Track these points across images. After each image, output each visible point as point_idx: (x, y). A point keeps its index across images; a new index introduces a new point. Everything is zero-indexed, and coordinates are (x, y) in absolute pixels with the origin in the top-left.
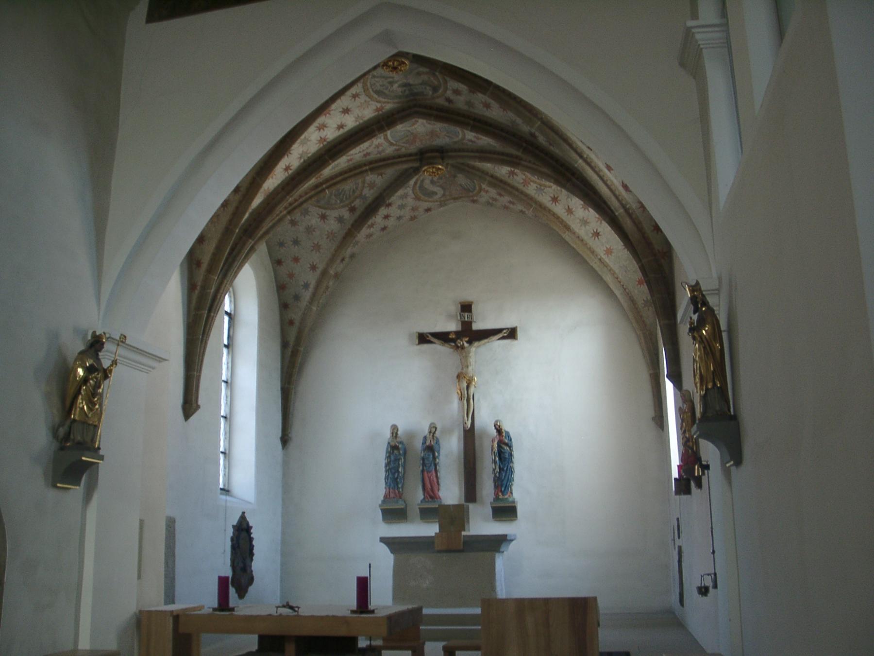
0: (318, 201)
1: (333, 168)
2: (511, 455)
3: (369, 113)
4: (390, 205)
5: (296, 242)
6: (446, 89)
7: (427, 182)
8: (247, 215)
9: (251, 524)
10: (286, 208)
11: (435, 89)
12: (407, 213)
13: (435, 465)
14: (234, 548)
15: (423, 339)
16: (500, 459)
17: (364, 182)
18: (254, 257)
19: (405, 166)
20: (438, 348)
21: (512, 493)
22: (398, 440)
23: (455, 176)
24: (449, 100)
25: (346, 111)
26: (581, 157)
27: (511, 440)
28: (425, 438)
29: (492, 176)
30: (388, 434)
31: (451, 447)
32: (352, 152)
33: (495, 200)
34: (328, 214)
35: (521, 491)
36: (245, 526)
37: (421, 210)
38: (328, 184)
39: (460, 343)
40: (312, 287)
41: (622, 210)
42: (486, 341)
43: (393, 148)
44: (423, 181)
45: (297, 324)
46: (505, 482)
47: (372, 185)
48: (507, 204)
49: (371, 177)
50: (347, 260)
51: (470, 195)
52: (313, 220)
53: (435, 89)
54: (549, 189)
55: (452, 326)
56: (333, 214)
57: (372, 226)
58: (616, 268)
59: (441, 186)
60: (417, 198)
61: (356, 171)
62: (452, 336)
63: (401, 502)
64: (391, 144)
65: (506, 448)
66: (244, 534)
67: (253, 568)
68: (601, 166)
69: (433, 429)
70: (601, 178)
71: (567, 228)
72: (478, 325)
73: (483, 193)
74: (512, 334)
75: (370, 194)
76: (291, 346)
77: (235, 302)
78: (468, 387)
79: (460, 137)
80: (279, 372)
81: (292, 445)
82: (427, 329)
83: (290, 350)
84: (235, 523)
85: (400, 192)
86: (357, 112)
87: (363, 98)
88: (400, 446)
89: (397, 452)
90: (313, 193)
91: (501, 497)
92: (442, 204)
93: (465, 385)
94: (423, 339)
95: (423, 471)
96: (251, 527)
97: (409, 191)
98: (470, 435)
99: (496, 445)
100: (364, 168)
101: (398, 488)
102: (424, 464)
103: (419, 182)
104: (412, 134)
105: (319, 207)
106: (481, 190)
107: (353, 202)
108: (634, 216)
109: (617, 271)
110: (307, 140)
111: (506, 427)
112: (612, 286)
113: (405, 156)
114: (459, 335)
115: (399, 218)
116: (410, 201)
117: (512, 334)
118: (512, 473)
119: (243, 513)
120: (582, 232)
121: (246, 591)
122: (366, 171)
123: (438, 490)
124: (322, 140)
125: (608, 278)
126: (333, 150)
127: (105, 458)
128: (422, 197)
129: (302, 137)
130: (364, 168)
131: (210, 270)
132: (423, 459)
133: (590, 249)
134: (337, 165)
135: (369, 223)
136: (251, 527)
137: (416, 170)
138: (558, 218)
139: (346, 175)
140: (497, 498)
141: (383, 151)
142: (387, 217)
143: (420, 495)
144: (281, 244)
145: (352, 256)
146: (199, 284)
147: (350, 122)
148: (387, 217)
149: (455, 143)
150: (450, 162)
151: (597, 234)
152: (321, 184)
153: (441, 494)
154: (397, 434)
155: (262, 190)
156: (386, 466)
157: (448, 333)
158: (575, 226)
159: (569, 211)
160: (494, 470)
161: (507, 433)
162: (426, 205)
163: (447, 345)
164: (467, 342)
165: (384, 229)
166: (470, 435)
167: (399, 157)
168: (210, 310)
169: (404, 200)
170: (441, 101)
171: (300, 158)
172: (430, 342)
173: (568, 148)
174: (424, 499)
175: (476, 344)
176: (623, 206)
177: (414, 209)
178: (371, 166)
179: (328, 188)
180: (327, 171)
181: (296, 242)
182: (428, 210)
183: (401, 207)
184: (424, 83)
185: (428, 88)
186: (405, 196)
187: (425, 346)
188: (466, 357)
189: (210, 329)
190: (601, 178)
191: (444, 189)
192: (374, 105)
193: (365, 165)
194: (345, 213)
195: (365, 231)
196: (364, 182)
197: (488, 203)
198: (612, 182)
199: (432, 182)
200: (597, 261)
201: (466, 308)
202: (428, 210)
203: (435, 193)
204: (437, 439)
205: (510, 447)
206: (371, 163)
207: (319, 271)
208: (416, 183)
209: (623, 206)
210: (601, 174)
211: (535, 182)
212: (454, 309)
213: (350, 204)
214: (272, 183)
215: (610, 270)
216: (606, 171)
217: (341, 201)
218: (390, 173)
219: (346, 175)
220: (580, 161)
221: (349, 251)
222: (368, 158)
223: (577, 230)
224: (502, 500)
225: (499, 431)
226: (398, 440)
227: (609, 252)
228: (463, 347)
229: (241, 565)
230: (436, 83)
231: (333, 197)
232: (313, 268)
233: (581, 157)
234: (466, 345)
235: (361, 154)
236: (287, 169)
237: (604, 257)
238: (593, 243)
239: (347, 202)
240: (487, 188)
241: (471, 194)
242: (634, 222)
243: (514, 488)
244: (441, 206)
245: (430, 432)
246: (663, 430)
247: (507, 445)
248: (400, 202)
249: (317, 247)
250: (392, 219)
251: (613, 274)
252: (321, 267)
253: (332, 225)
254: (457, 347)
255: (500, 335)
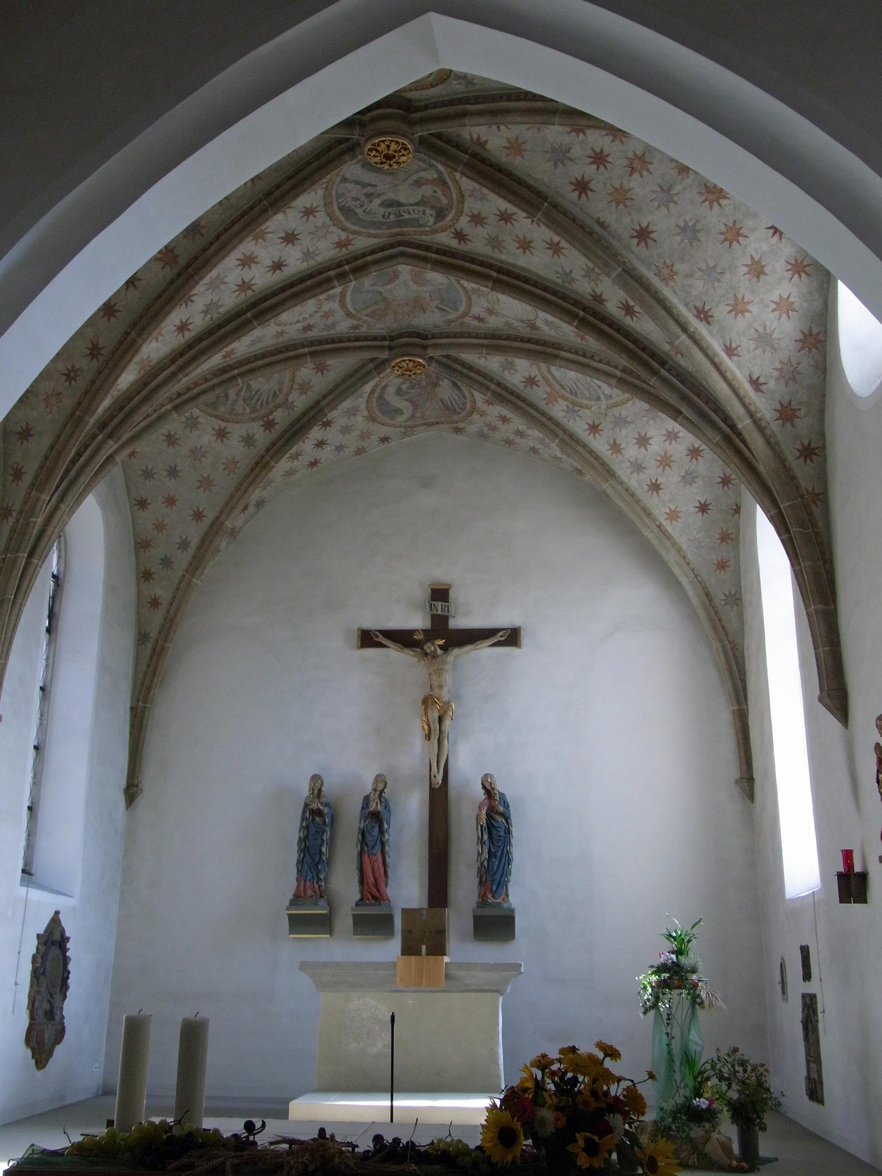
0: (214, 405)
1: (253, 343)
2: (508, 832)
3: (326, 250)
4: (327, 424)
5: (173, 472)
6: (460, 213)
7: (391, 390)
8: (107, 402)
9: (67, 934)
10: (171, 400)
11: (440, 214)
12: (352, 441)
13: (383, 844)
14: (36, 975)
15: (368, 639)
16: (490, 837)
17: (293, 380)
18: (101, 486)
19: (367, 355)
20: (394, 654)
21: (507, 896)
22: (323, 800)
23: (436, 385)
24: (460, 236)
25: (290, 238)
26: (685, 330)
27: (507, 807)
28: (367, 799)
29: (499, 384)
30: (304, 790)
31: (410, 812)
32: (284, 317)
33: (493, 428)
34: (229, 429)
35: (522, 893)
36: (57, 937)
37: (374, 438)
38: (242, 369)
39: (429, 647)
40: (193, 545)
41: (748, 421)
42: (470, 647)
43: (350, 322)
44: (385, 387)
45: (164, 604)
46: (497, 877)
47: (305, 388)
48: (512, 437)
49: (306, 372)
50: (251, 509)
51: (453, 417)
52: (205, 438)
53: (440, 214)
54: (587, 411)
55: (416, 621)
56: (237, 430)
57: (296, 456)
58: (683, 541)
59: (410, 400)
60: (371, 418)
61: (287, 354)
62: (419, 637)
63: (322, 903)
64: (349, 315)
65: (500, 819)
66: (55, 951)
67: (65, 1013)
68: (717, 347)
69: (381, 782)
70: (717, 367)
71: (610, 473)
72: (459, 622)
73: (475, 417)
74: (512, 637)
75: (300, 402)
76: (152, 641)
77: (64, 559)
78: (441, 720)
79: (462, 309)
80: (130, 681)
81: (142, 802)
82: (372, 623)
83: (149, 646)
84: (41, 931)
85: (347, 404)
86: (305, 241)
87: (321, 218)
88: (326, 810)
89: (317, 820)
90: (215, 381)
91: (491, 900)
92: (408, 430)
93: (436, 715)
94: (368, 639)
95: (361, 854)
96: (68, 939)
97: (362, 403)
98: (439, 798)
99: (484, 812)
100: (301, 351)
101: (319, 879)
102: (363, 841)
103: (378, 390)
104: (385, 299)
105: (217, 417)
106: (474, 409)
107: (272, 413)
108: (768, 432)
109: (684, 547)
110: (220, 281)
111: (500, 786)
112: (676, 570)
113: (366, 339)
114: (430, 634)
115: (340, 448)
116: (360, 421)
117: (512, 637)
118: (509, 861)
119: (57, 913)
120: (634, 481)
121: (50, 1054)
122: (304, 355)
123: (386, 885)
124: (244, 286)
125: (670, 557)
126: (260, 307)
127: (355, 640)
128: (381, 417)
129: (213, 274)
130: (301, 351)
131: (39, 484)
132: (363, 833)
133: (644, 509)
134: (260, 339)
135: (293, 451)
136: (68, 939)
137: (380, 366)
138: (597, 458)
139: (272, 359)
140: (483, 902)
141: (334, 325)
142: (320, 444)
143: (354, 893)
144: (148, 474)
145: (260, 504)
146: (17, 507)
147: (295, 262)
148: (320, 444)
149: (450, 321)
150: (436, 353)
151: (655, 487)
152: (231, 368)
153: (390, 891)
154: (320, 790)
155: (137, 359)
156: (299, 843)
157: (410, 633)
158: (623, 471)
159: (616, 447)
160: (480, 855)
161: (502, 796)
162: (383, 431)
163: (407, 651)
164: (441, 647)
165: (313, 464)
166: (439, 798)
167: (357, 339)
168: (31, 555)
169: (351, 416)
170: (445, 239)
171: (205, 312)
172: (381, 645)
173: (664, 313)
174: (362, 899)
175: (456, 651)
176: (751, 415)
177: (364, 436)
178: (313, 349)
179: (241, 375)
180: (242, 346)
181: (173, 472)
182: (385, 440)
183: (345, 430)
184: (422, 202)
185: (429, 211)
186: (352, 412)
187: (371, 652)
188: (439, 672)
189: (29, 587)
190: (717, 367)
191: (415, 406)
192: (337, 235)
193: (303, 346)
194: (257, 430)
195: (284, 465)
196: (293, 380)
197: (481, 435)
198: (733, 373)
199: (399, 392)
200: (654, 527)
201: (440, 594)
202: (385, 440)
203: (399, 411)
204: (386, 800)
205: (507, 818)
206: (312, 343)
207: (207, 522)
208: (373, 391)
209: (751, 415)
210: (717, 360)
211: (566, 400)
212: (422, 594)
213: (267, 415)
214: (156, 347)
215: (674, 544)
216: (723, 355)
217: (254, 410)
218: (339, 366)
219: (272, 359)
220: (684, 337)
221: (256, 495)
222: (310, 334)
223: (625, 479)
224: (492, 905)
225: (489, 792)
226: (323, 800)
227: (673, 515)
228: (434, 656)
229: (46, 1006)
230: (445, 201)
231: (241, 402)
232: (198, 516)
233: (685, 330)
234: (439, 652)
235: (299, 326)
236: (182, 327)
237: (664, 523)
238: (651, 501)
239: (262, 412)
240: (484, 407)
241: (455, 417)
242: (768, 441)
243: (511, 888)
244: (405, 434)
245: (375, 790)
246: (753, 802)
247: (502, 815)
248: (343, 421)
249: (206, 483)
250: (327, 448)
251: (679, 550)
252: (210, 515)
253: (235, 448)
254: (426, 654)
255: (494, 640)
